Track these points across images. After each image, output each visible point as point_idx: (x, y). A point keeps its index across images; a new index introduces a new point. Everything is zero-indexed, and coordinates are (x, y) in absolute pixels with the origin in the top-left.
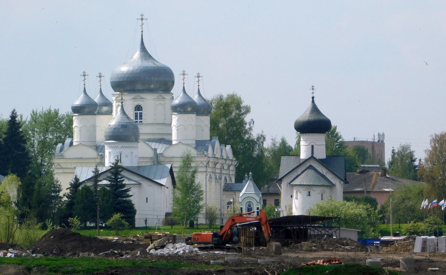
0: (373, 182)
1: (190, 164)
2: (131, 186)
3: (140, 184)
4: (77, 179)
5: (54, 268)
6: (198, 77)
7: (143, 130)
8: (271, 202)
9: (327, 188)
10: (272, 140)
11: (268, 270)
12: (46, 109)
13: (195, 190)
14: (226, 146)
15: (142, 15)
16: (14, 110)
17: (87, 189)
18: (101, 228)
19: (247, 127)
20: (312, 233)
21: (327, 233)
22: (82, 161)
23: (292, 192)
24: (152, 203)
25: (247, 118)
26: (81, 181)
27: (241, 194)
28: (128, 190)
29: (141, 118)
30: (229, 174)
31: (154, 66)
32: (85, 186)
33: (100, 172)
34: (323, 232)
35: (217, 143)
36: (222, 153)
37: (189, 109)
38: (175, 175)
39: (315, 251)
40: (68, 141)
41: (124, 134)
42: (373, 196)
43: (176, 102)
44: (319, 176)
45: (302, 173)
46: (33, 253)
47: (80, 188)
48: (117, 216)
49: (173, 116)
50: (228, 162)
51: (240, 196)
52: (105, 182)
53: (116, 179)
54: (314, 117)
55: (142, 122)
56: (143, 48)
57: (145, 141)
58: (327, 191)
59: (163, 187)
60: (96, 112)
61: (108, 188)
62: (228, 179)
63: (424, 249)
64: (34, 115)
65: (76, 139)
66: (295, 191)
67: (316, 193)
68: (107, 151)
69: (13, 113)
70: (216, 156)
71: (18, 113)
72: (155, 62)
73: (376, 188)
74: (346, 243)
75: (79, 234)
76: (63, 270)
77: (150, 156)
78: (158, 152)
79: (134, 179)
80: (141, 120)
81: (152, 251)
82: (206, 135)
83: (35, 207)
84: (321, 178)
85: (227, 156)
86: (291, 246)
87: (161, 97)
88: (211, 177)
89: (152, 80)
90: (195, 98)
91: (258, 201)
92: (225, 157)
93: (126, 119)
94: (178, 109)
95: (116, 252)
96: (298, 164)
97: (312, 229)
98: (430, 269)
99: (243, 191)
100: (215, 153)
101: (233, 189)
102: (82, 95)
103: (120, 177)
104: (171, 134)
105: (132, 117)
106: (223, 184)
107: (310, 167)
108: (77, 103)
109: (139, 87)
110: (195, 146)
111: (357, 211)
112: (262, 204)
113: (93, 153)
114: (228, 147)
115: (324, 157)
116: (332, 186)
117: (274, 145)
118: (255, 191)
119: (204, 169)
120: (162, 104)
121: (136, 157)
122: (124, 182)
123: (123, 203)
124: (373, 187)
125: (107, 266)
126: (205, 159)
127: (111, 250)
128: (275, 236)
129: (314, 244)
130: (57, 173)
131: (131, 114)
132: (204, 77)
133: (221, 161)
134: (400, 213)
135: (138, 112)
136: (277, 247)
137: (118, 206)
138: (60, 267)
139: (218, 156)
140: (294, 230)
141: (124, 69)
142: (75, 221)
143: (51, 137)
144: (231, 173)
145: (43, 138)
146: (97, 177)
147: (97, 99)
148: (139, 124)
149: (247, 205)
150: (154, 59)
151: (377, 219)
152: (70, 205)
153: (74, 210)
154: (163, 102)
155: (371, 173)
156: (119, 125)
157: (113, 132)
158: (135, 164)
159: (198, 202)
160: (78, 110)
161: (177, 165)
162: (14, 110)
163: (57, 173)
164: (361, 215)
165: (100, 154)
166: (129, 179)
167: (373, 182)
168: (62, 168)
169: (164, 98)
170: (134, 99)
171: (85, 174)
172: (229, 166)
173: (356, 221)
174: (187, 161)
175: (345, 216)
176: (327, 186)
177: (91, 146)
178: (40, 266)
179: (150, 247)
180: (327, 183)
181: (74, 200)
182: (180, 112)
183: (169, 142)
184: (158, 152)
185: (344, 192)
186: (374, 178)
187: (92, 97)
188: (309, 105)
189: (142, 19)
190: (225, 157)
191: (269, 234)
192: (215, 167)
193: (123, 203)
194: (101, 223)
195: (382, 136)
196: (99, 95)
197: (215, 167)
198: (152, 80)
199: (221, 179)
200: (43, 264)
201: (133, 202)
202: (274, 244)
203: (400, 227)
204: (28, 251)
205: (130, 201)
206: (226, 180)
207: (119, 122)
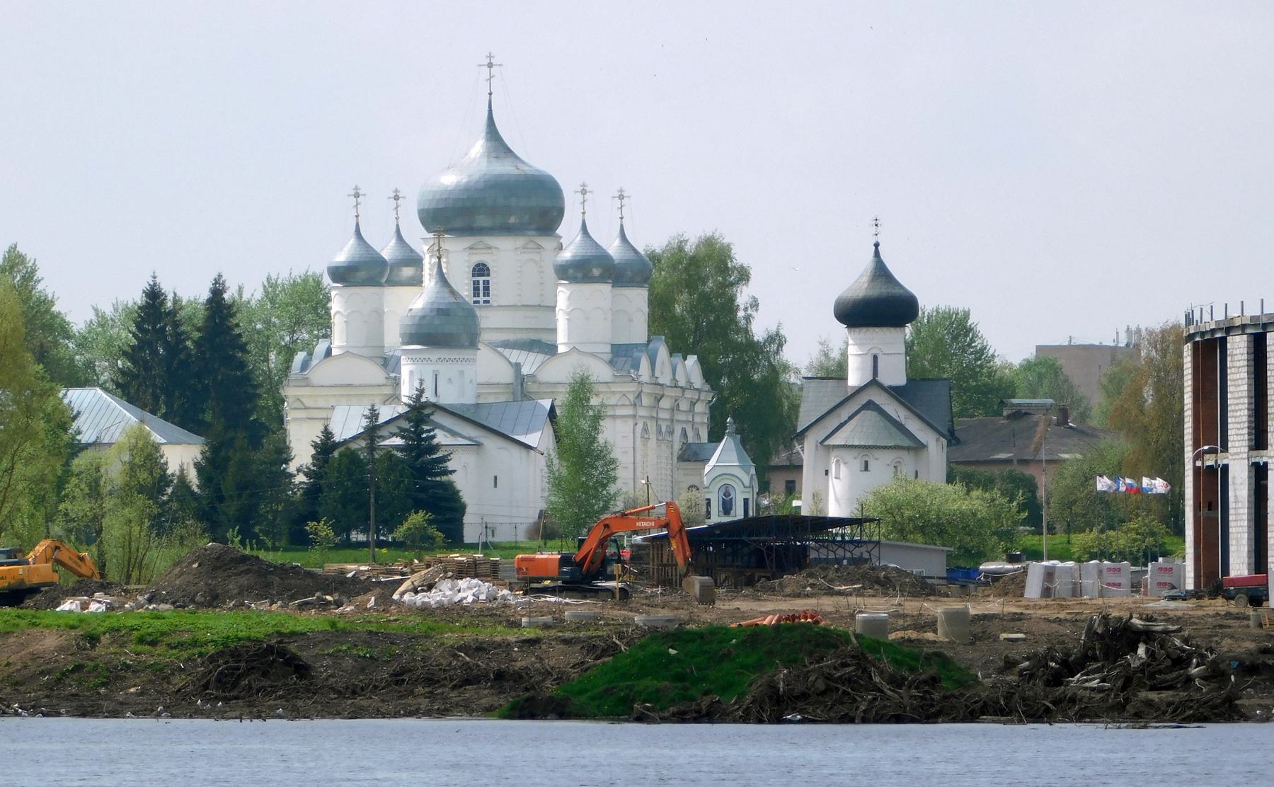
1: (588, 400)
2: (451, 449)
3: (479, 445)
4: (327, 434)
5: (150, 634)
6: (621, 197)
7: (489, 320)
8: (778, 484)
9: (905, 453)
10: (821, 344)
11: (620, 638)
12: (298, 273)
13: (598, 458)
14: (685, 359)
15: (490, 57)
16: (220, 276)
17: (351, 457)
18: (381, 544)
19: (741, 314)
22: (348, 390)
23: (828, 463)
24: (504, 488)
25: (743, 297)
26: (337, 439)
27: (707, 468)
28: (444, 459)
29: (487, 294)
30: (693, 423)
31: (517, 172)
32: (348, 449)
34: (840, 552)
35: (663, 352)
36: (674, 374)
37: (596, 272)
39: (807, 596)
40: (321, 346)
41: (444, 331)
42: (1029, 471)
43: (567, 255)
44: (888, 424)
45: (850, 418)
46: (150, 601)
47: (336, 454)
48: (417, 519)
49: (560, 288)
53: (418, 433)
54: (880, 290)
55: (487, 302)
56: (492, 132)
57: (494, 346)
58: (907, 459)
61: (399, 454)
63: (1047, 592)
64: (271, 291)
65: (338, 340)
66: (833, 460)
67: (882, 466)
68: (406, 369)
69: (216, 281)
70: (660, 381)
71: (167, 288)
72: (520, 165)
74: (885, 577)
75: (257, 557)
76: (167, 640)
77: (503, 381)
78: (525, 370)
79: (464, 434)
81: (406, 597)
82: (638, 331)
83: (231, 497)
84: (894, 430)
85: (689, 382)
86: (759, 584)
87: (532, 245)
88: (645, 430)
89: (512, 205)
90: (613, 248)
91: (747, 484)
92: (682, 383)
93: (447, 295)
94: (571, 271)
95: (329, 598)
98: (1004, 635)
99: (713, 461)
100: (657, 374)
102: (352, 241)
103: (425, 428)
104: (554, 331)
105: (466, 292)
106: (677, 446)
107: (870, 405)
108: (341, 258)
109: (482, 221)
110: (609, 357)
111: (965, 506)
112: (756, 490)
113: (376, 374)
114: (692, 360)
115: (900, 380)
116: (918, 447)
117: (826, 355)
118: (740, 460)
119: (630, 411)
120: (535, 261)
122: (435, 441)
123: (433, 487)
124: (1037, 450)
125: (270, 630)
126: (633, 387)
127: (318, 594)
128: (696, 566)
129: (811, 581)
130: (295, 419)
131: (463, 285)
132: (635, 200)
133: (668, 392)
134: (1077, 509)
135: (481, 279)
136: (703, 586)
137: (421, 496)
138: (163, 634)
139: (665, 379)
141: (450, 180)
142: (322, 529)
143: (306, 336)
144: (698, 419)
145: (287, 339)
146: (372, 431)
147: (388, 251)
148: (480, 307)
150: (516, 157)
151: (1016, 523)
152: (313, 492)
153: (320, 504)
154: (536, 257)
155: (1035, 418)
156: (432, 310)
157: (419, 325)
158: (469, 399)
159: (604, 486)
160: (343, 275)
161: (562, 398)
162: (220, 276)
163: (295, 419)
164: (974, 514)
165: (393, 375)
166: (454, 434)
168: (306, 408)
169: (540, 247)
170: (471, 248)
171: (347, 424)
172: (693, 404)
173: (963, 528)
174: (581, 390)
175: (938, 518)
176: (908, 449)
177: (371, 358)
178: (118, 630)
179: (402, 588)
180: (907, 442)
181: (322, 482)
182: (574, 280)
183: (551, 349)
184: (525, 370)
186: (1040, 428)
187: (377, 248)
189: (490, 65)
191: (686, 559)
193: (433, 487)
194: (384, 535)
196: (394, 241)
198: (512, 205)
199: (671, 433)
200: (125, 627)
201: (458, 486)
202: (697, 582)
203: (1069, 542)
204: (140, 598)
205: (449, 487)
206: (684, 434)
207: (432, 303)
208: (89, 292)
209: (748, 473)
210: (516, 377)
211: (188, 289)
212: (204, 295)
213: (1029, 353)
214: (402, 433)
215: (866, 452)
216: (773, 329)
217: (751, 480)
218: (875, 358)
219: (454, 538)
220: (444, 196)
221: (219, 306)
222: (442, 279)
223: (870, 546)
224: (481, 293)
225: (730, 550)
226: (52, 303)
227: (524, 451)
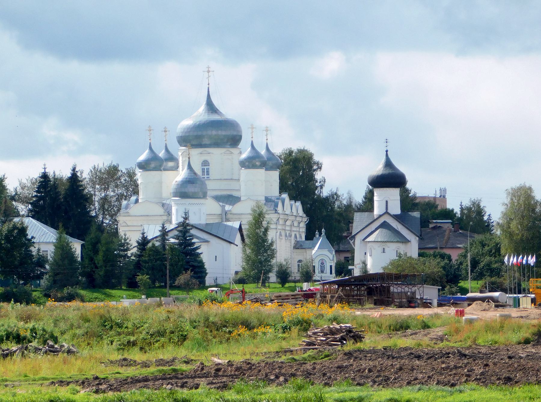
0: (445, 238)
20: (395, 290)
21: (410, 290)
25: (318, 176)
29: (208, 174)
33: (167, 231)
34: (407, 289)
38: (245, 233)
43: (244, 156)
50: (299, 219)
51: (313, 253)
52: (172, 240)
55: (209, 177)
59: (232, 245)
60: (162, 168)
73: (449, 244)
87: (228, 152)
88: (281, 235)
90: (263, 152)
93: (193, 175)
96: (372, 220)
97: (395, 286)
101: (304, 247)
102: (147, 151)
106: (293, 242)
108: (142, 157)
114: (299, 204)
121: (204, 213)
122: (193, 241)
135: (205, 167)
139: (288, 211)
140: (377, 287)
144: (301, 230)
147: (162, 154)
149: (320, 263)
160: (144, 166)
167: (445, 238)
169: (232, 153)
172: (299, 223)
177: (157, 203)
182: (248, 167)
185: (419, 249)
186: (447, 233)
188: (383, 160)
189: (209, 72)
190: (295, 214)
192: (285, 225)
195: (443, 191)
196: (250, 149)
197: (285, 225)
199: (290, 236)
208: (20, 175)
209: (332, 254)
210: (222, 211)
214: (177, 237)
215: (384, 244)
216: (334, 190)
217: (333, 257)
218: (387, 202)
219: (202, 286)
220: (186, 130)
222: (190, 167)
224: (206, 173)
225: (356, 288)
227: (228, 244)
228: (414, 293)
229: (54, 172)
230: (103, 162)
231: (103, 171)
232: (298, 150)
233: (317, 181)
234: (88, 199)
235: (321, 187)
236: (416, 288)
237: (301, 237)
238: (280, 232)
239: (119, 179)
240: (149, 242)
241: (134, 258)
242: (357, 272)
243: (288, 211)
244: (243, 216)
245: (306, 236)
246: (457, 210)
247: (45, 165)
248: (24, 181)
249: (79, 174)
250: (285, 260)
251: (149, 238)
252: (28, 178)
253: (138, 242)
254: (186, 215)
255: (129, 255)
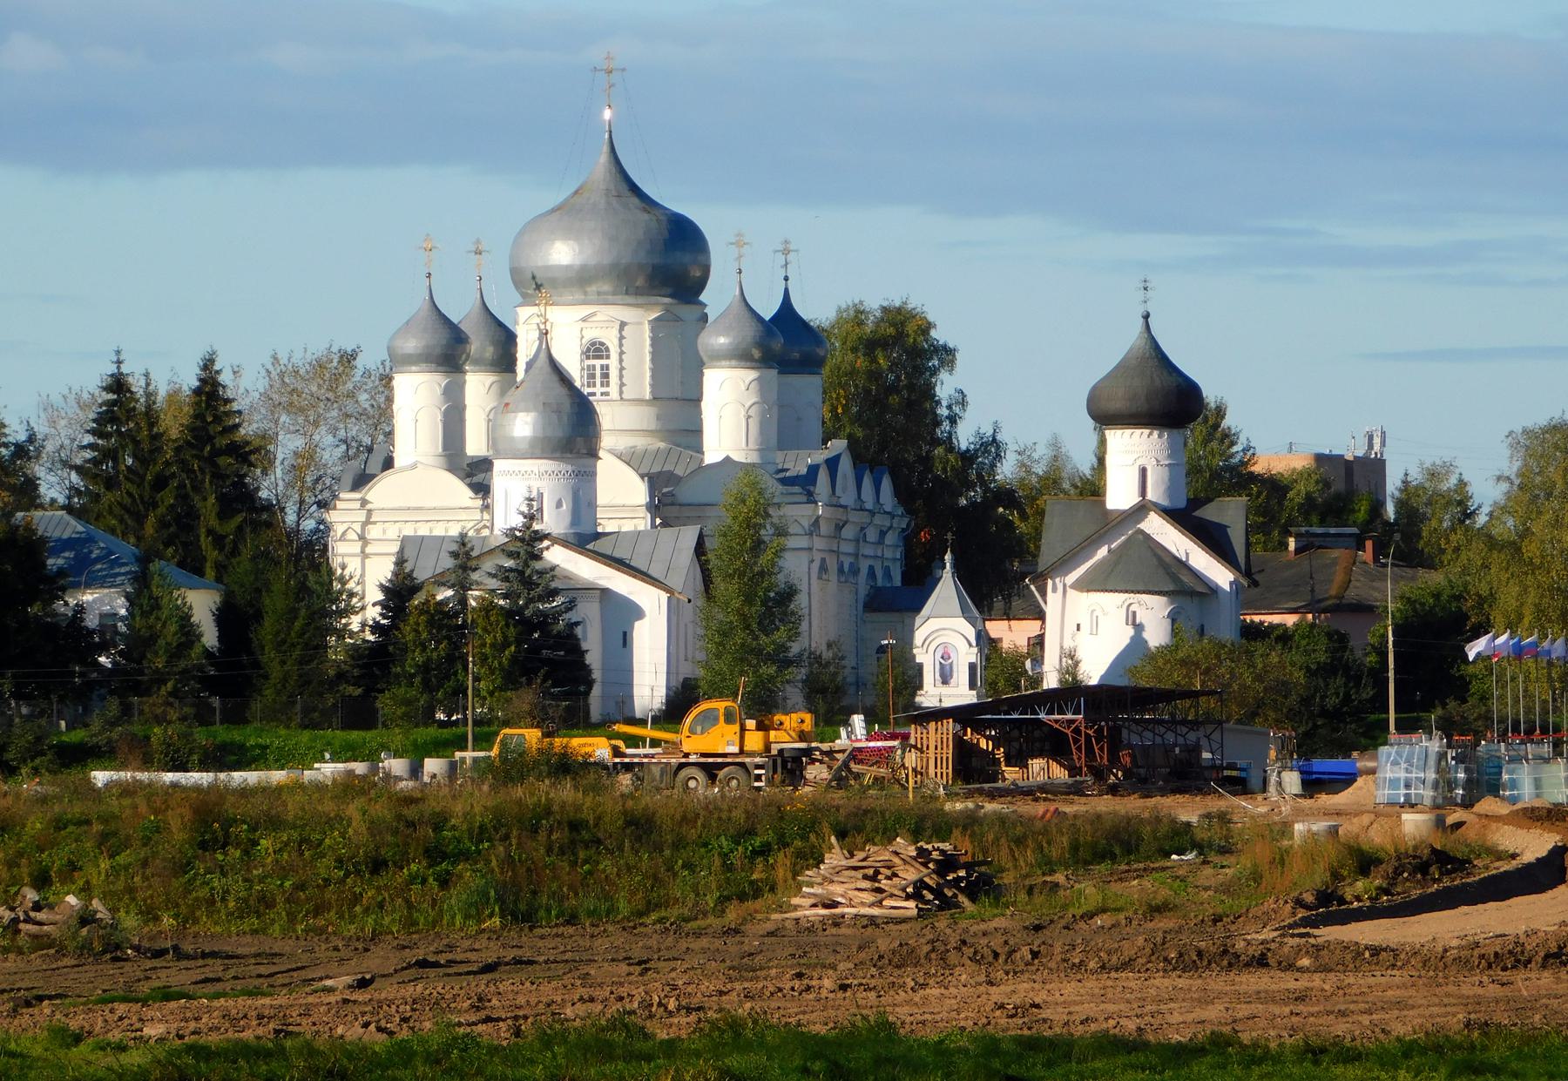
21: (1181, 740)
25: (945, 386)
55: (607, 394)
62: (879, 574)
70: (843, 502)
71: (134, 370)
80: (604, 390)
92: (869, 505)
97: (1134, 727)
100: (838, 492)
106: (863, 590)
133: (855, 517)
135: (598, 363)
172: (883, 534)
190: (869, 505)
199: (855, 571)
211: (168, 374)
212: (189, 379)
213: (1299, 462)
216: (988, 431)
221: (209, 392)
223: (1210, 728)
226: (1373, 467)
228: (1196, 750)
229: (147, 375)
230: (305, 341)
231: (302, 372)
232: (885, 310)
233: (938, 403)
234: (249, 454)
235: (953, 420)
236: (1201, 733)
237: (887, 574)
238: (823, 560)
239: (351, 395)
240: (415, 589)
241: (371, 638)
242: (1051, 681)
243: (848, 498)
244: (710, 512)
245: (903, 574)
246: (1487, 479)
247: (118, 352)
248: (56, 399)
249: (222, 378)
250: (829, 646)
251: (421, 575)
252: (66, 392)
253: (383, 588)
254: (530, 506)
255: (355, 627)
